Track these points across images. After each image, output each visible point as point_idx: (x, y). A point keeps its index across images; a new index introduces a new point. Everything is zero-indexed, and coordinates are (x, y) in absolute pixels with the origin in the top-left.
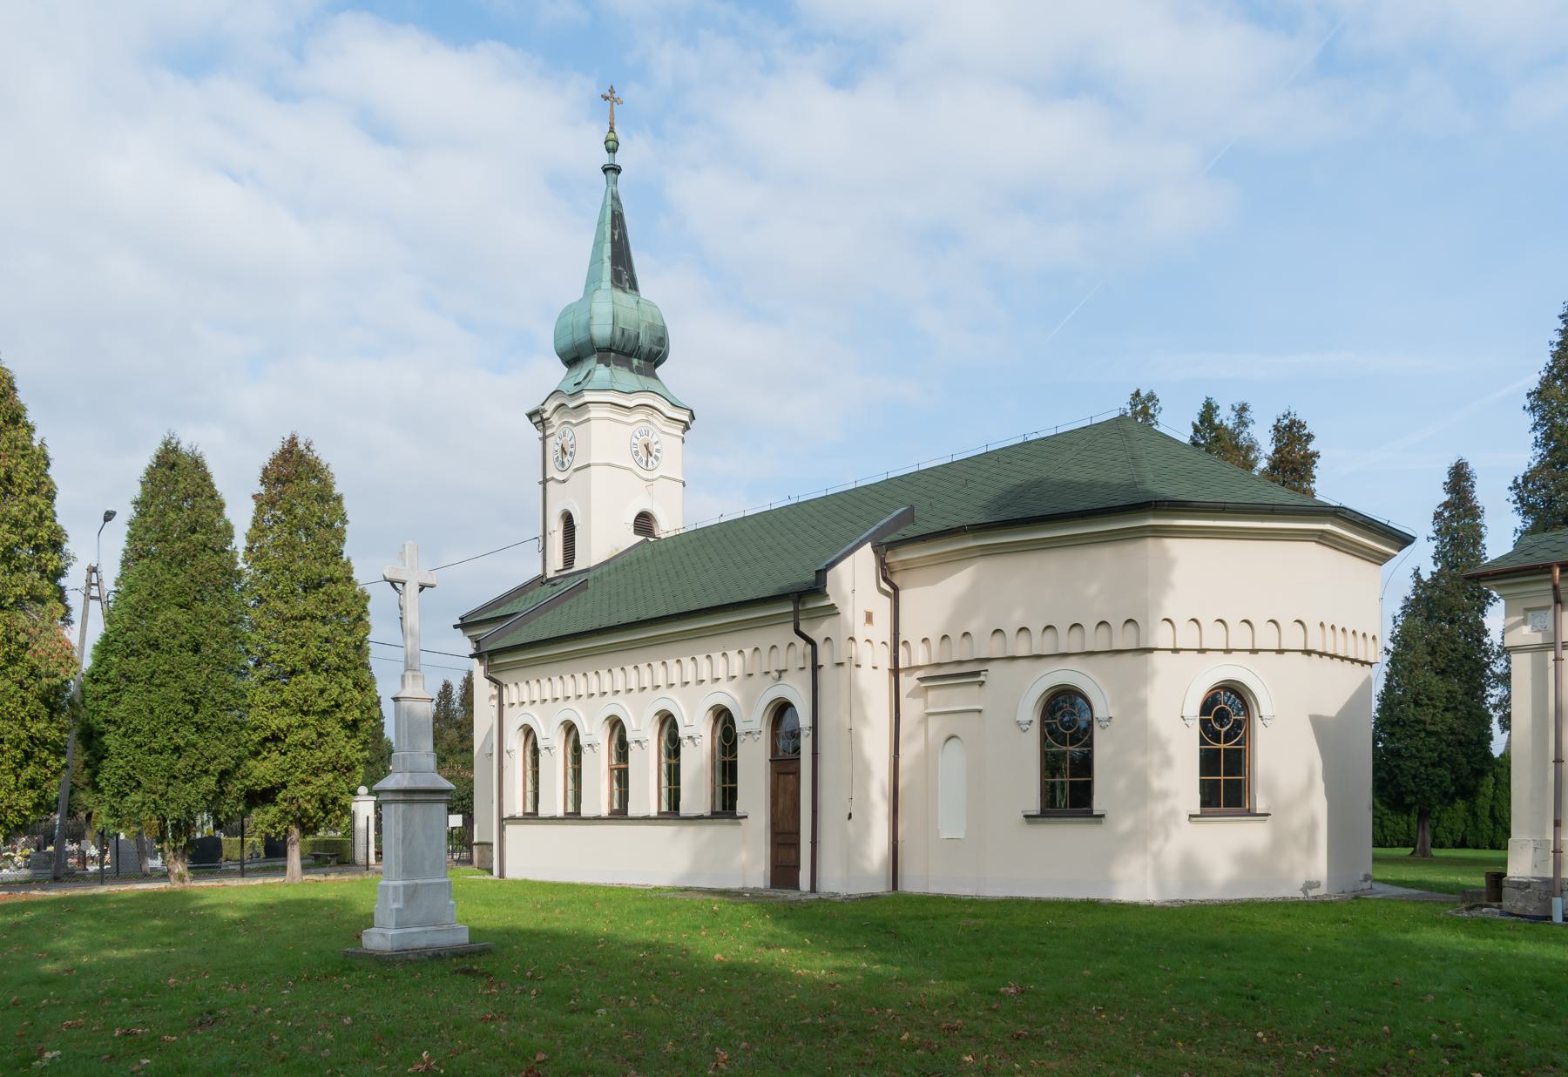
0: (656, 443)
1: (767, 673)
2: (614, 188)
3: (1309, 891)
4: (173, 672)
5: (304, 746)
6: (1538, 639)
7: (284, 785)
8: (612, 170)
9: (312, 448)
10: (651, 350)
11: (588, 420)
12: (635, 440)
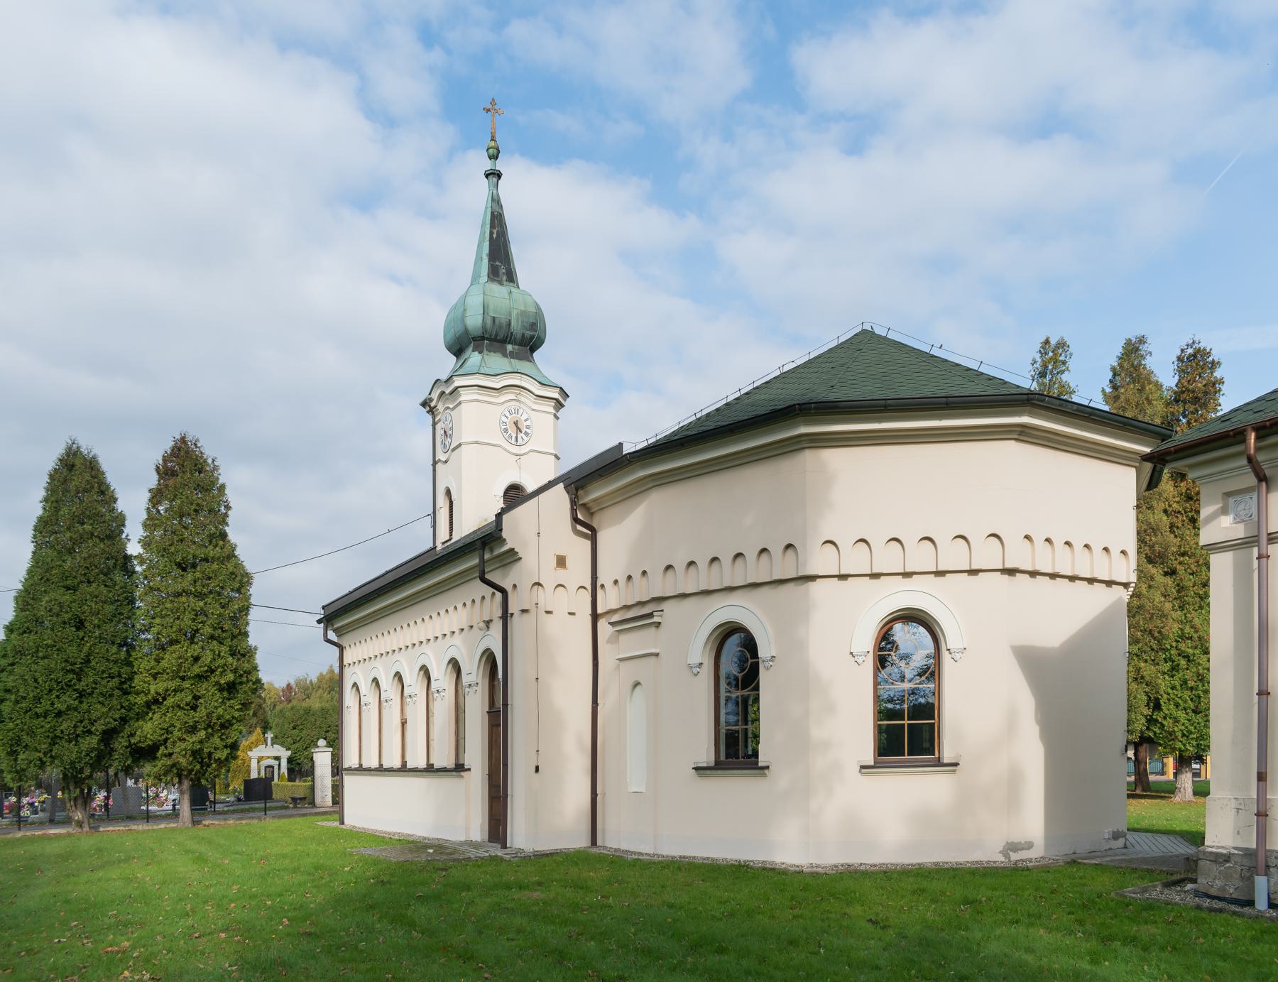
0: (526, 420)
2: (495, 192)
3: (1011, 853)
4: (55, 646)
6: (1240, 532)
7: (166, 740)
8: (494, 175)
9: (199, 445)
10: (523, 335)
11: (460, 403)
12: (504, 419)
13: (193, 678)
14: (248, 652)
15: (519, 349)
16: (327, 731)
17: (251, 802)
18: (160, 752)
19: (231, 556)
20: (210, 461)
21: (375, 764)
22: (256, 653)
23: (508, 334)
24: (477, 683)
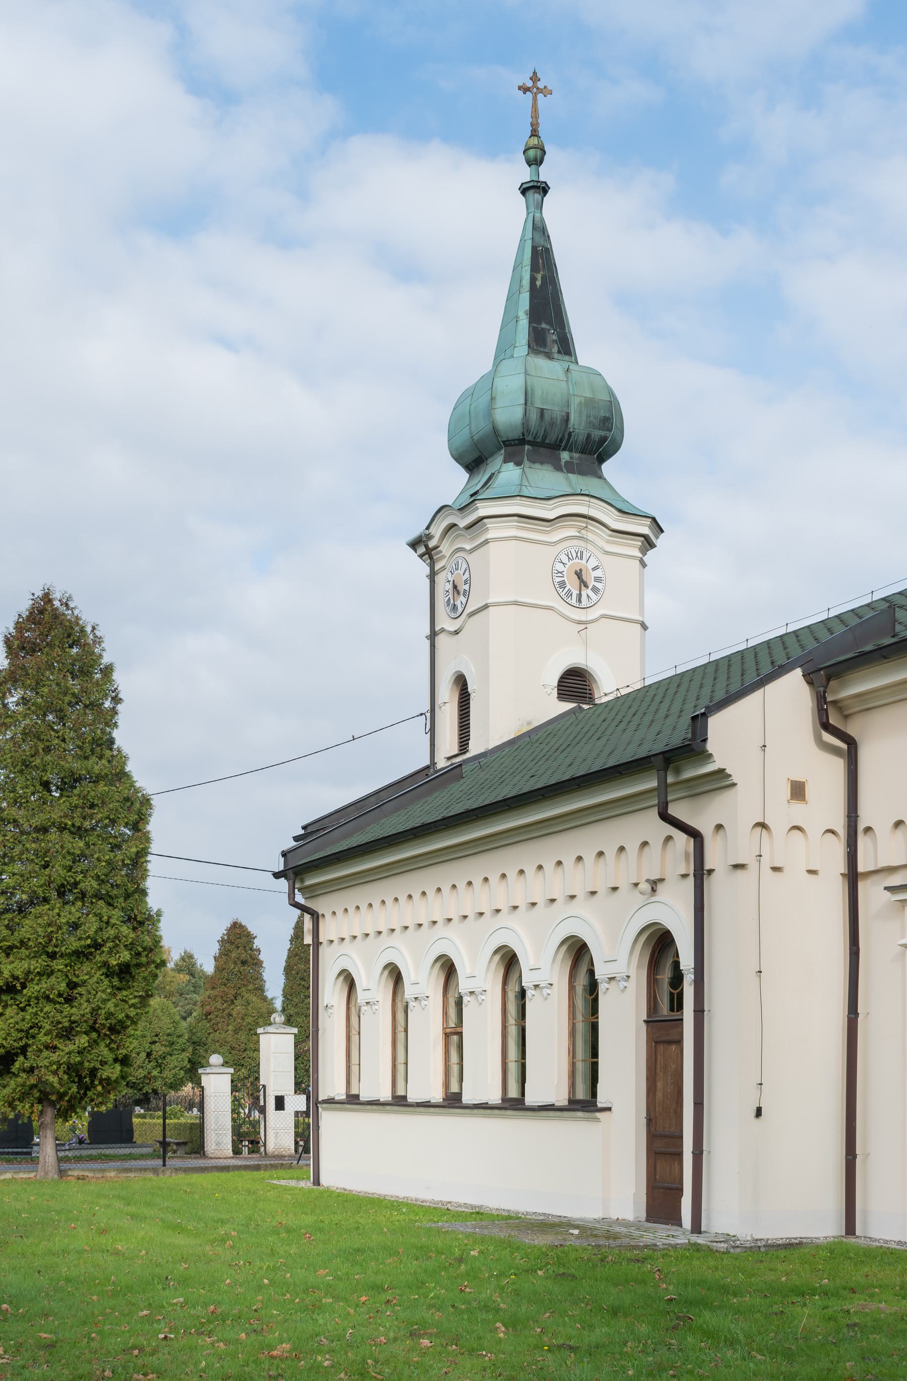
0: (594, 569)
1: (636, 885)
2: (538, 215)
5: (47, 998)
7: (24, 1050)
9: (71, 605)
10: (589, 436)
11: (486, 542)
12: (560, 567)
13: (70, 955)
14: (148, 919)
15: (580, 458)
16: (154, 1043)
17: (102, 1146)
18: (17, 1065)
19: (122, 776)
20: (89, 629)
21: (385, 1095)
22: (159, 921)
23: (563, 436)
24: (628, 977)
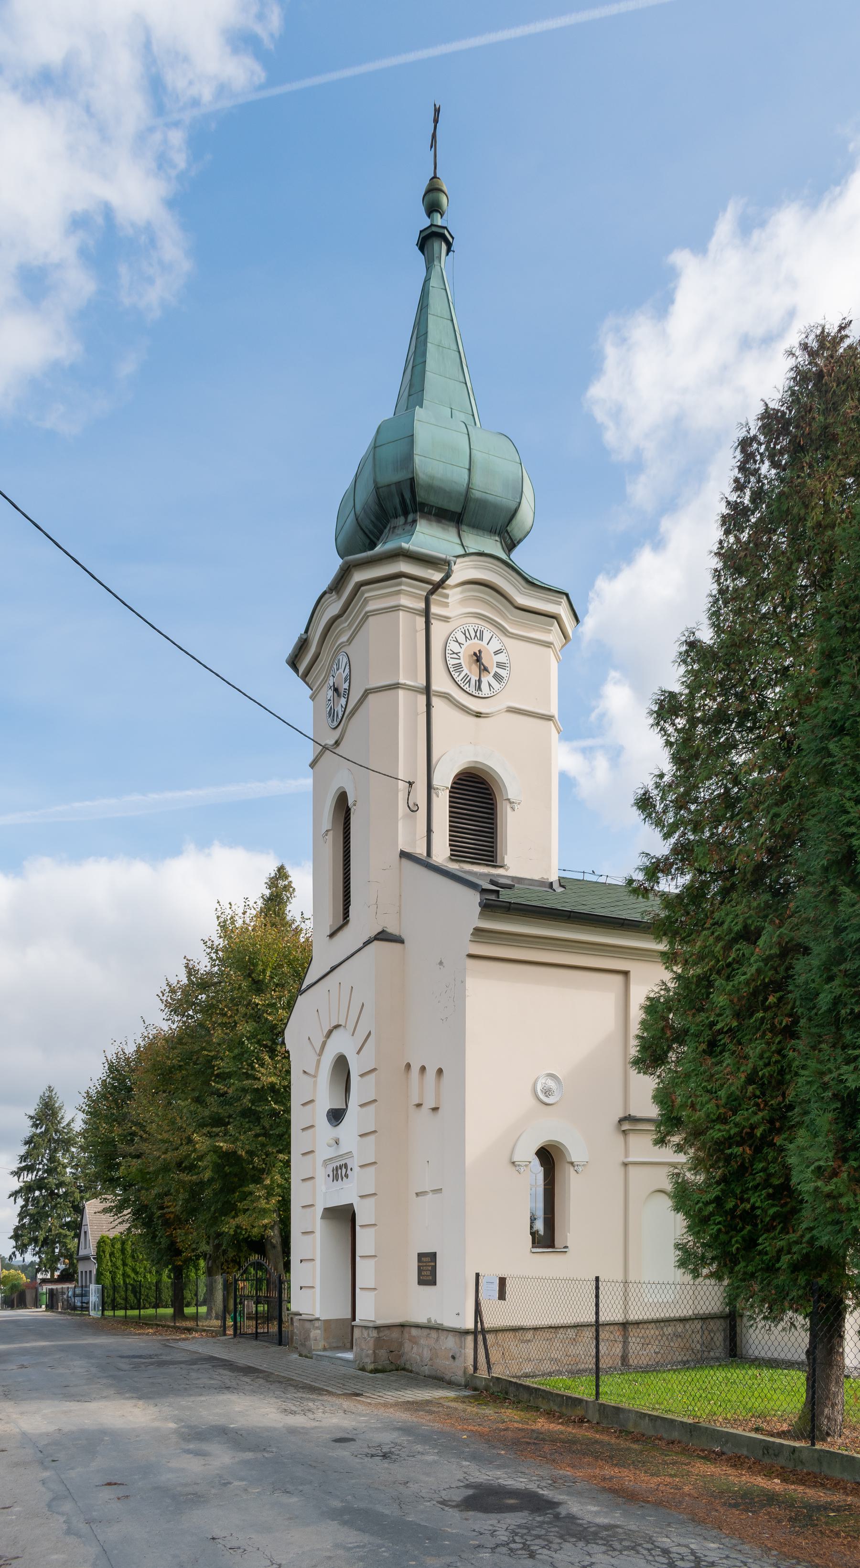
0: (496, 653)
